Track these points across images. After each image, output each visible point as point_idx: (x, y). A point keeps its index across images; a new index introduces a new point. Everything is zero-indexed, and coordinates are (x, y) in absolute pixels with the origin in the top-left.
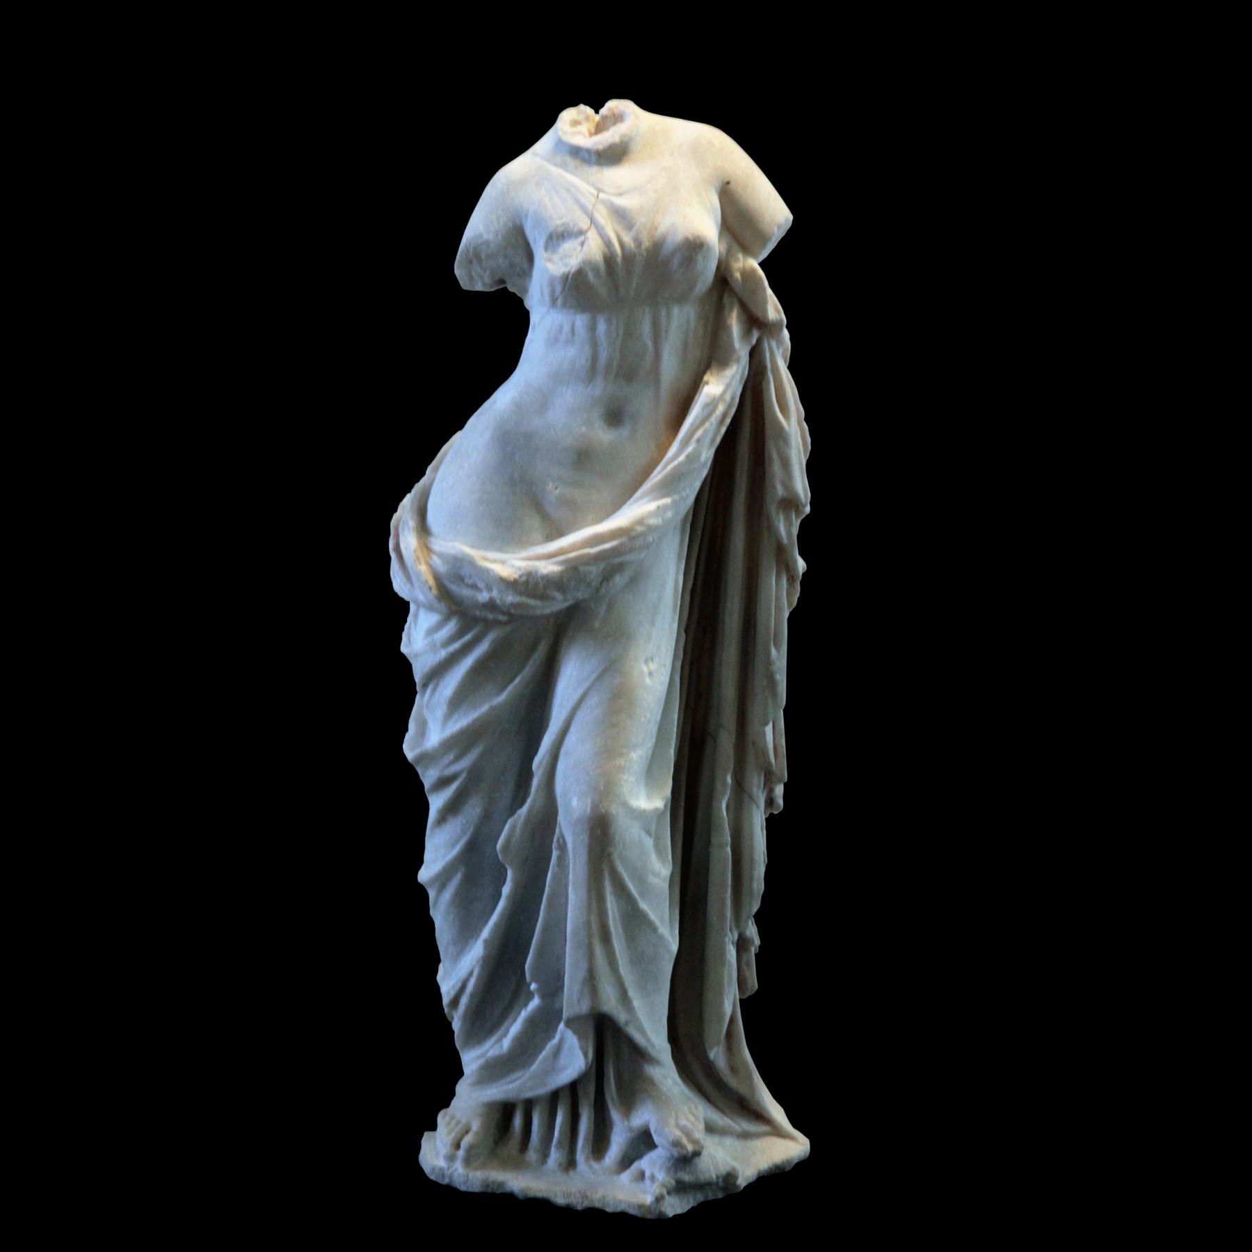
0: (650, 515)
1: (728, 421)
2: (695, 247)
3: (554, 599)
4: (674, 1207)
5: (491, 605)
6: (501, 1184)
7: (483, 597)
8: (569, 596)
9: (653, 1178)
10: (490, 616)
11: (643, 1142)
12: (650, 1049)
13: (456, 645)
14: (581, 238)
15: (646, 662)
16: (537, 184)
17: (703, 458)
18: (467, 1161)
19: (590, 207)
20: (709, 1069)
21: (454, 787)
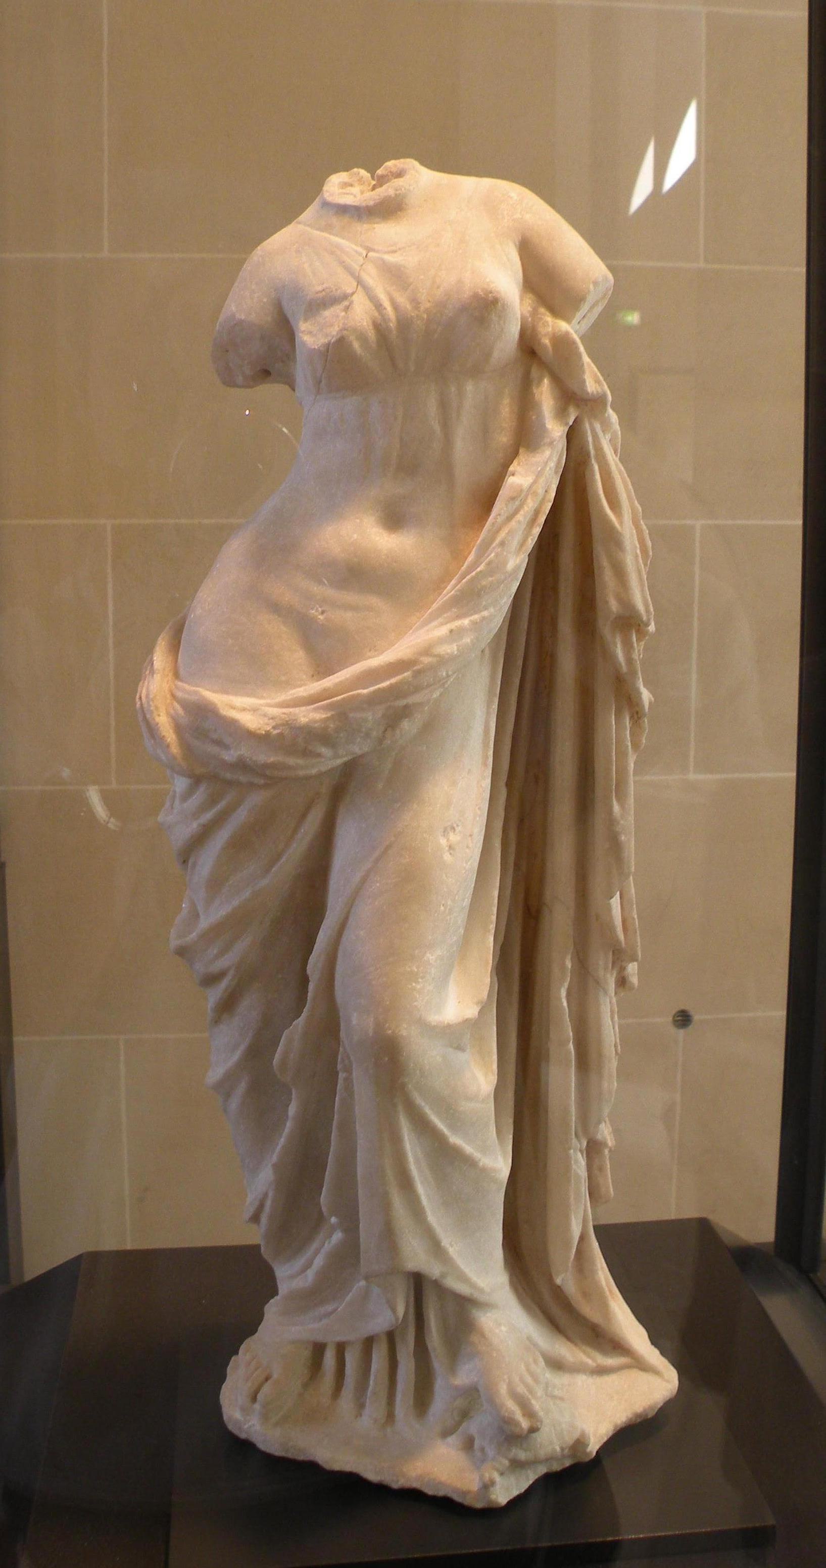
0: (441, 641)
1: (542, 519)
2: (486, 306)
3: (319, 755)
5: (242, 765)
7: (229, 756)
8: (341, 752)
10: (243, 779)
12: (476, 1295)
13: (209, 816)
14: (346, 303)
15: (445, 832)
16: (298, 251)
17: (511, 565)
19: (357, 268)
20: (558, 1293)
21: (224, 984)
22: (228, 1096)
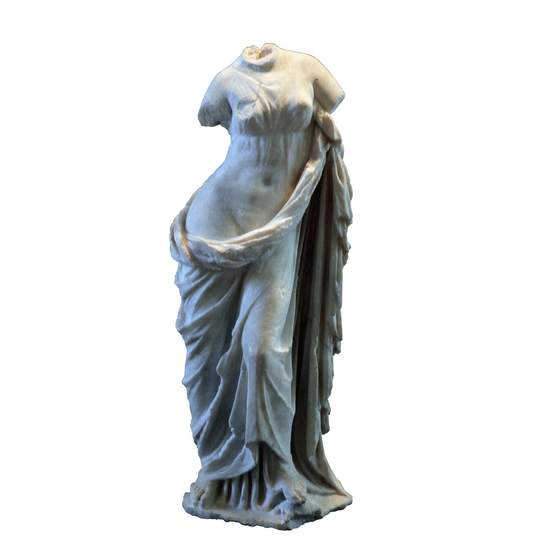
0: (283, 224)
1: (317, 183)
2: (302, 107)
3: (241, 261)
5: (214, 264)
7: (210, 260)
8: (248, 260)
9: (284, 513)
10: (213, 268)
11: (280, 497)
12: (283, 457)
13: (199, 281)
14: (253, 104)
15: (281, 288)
16: (234, 80)
17: (306, 199)
18: (203, 505)
19: (257, 90)
20: (309, 465)
21: (198, 342)
22: (193, 386)
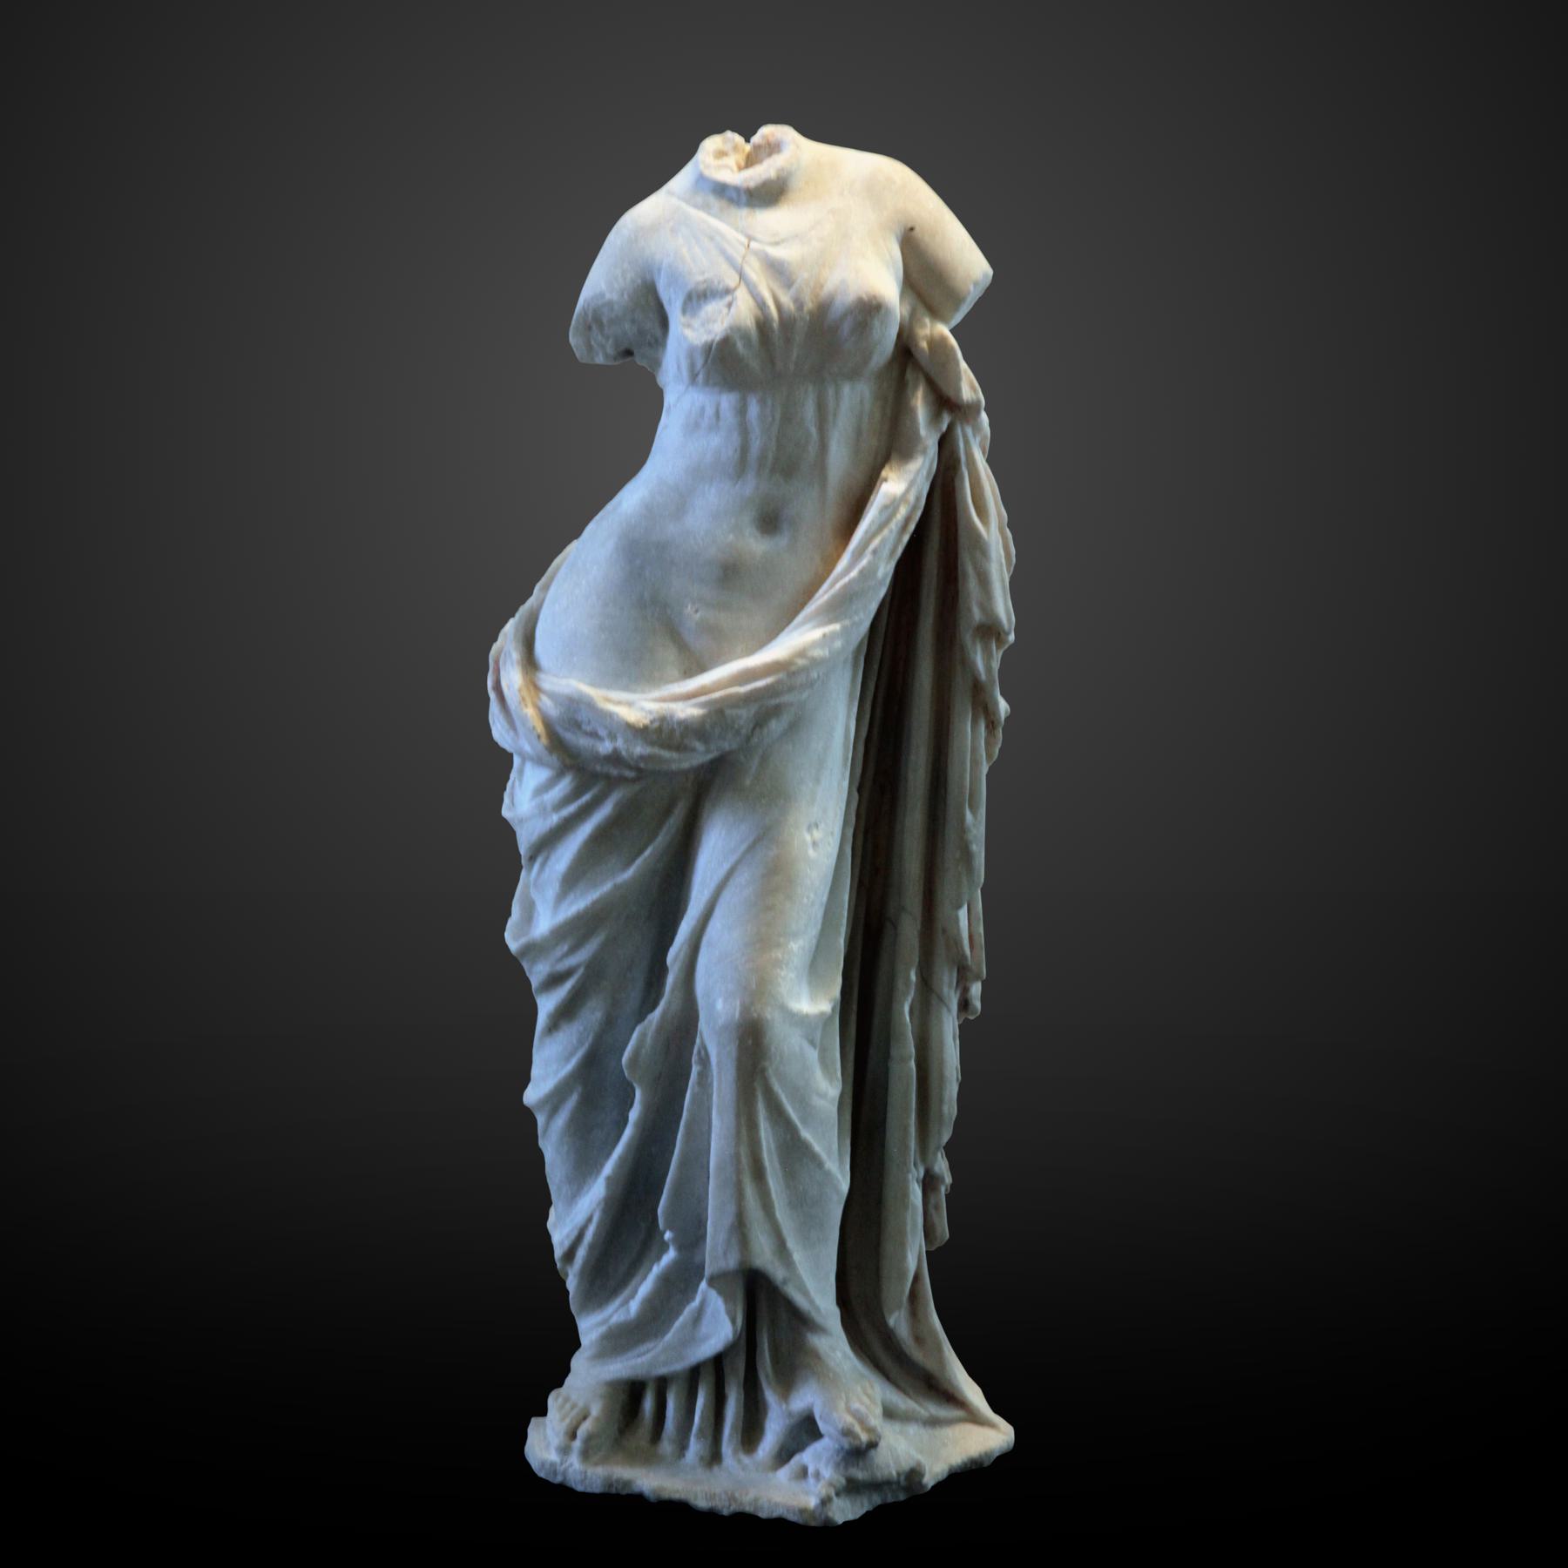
0: (814, 644)
1: (912, 527)
2: (870, 309)
3: (694, 750)
4: (845, 1511)
5: (615, 758)
6: (628, 1483)
7: (605, 747)
8: (712, 747)
9: (817, 1475)
10: (614, 772)
11: (806, 1430)
12: (814, 1314)
13: (572, 808)
14: (728, 299)
15: (809, 829)
16: (673, 231)
17: (880, 573)
18: (585, 1454)
19: (739, 260)
20: (888, 1338)
21: (568, 985)
